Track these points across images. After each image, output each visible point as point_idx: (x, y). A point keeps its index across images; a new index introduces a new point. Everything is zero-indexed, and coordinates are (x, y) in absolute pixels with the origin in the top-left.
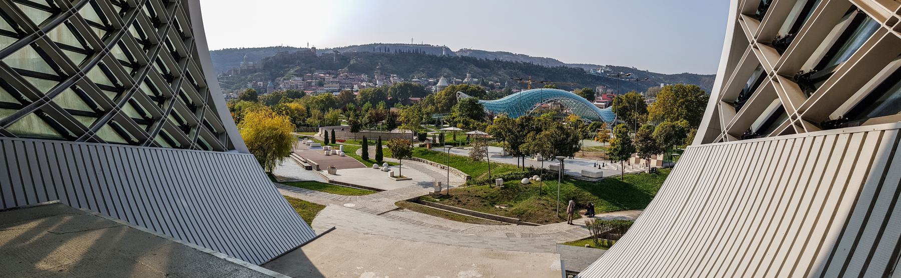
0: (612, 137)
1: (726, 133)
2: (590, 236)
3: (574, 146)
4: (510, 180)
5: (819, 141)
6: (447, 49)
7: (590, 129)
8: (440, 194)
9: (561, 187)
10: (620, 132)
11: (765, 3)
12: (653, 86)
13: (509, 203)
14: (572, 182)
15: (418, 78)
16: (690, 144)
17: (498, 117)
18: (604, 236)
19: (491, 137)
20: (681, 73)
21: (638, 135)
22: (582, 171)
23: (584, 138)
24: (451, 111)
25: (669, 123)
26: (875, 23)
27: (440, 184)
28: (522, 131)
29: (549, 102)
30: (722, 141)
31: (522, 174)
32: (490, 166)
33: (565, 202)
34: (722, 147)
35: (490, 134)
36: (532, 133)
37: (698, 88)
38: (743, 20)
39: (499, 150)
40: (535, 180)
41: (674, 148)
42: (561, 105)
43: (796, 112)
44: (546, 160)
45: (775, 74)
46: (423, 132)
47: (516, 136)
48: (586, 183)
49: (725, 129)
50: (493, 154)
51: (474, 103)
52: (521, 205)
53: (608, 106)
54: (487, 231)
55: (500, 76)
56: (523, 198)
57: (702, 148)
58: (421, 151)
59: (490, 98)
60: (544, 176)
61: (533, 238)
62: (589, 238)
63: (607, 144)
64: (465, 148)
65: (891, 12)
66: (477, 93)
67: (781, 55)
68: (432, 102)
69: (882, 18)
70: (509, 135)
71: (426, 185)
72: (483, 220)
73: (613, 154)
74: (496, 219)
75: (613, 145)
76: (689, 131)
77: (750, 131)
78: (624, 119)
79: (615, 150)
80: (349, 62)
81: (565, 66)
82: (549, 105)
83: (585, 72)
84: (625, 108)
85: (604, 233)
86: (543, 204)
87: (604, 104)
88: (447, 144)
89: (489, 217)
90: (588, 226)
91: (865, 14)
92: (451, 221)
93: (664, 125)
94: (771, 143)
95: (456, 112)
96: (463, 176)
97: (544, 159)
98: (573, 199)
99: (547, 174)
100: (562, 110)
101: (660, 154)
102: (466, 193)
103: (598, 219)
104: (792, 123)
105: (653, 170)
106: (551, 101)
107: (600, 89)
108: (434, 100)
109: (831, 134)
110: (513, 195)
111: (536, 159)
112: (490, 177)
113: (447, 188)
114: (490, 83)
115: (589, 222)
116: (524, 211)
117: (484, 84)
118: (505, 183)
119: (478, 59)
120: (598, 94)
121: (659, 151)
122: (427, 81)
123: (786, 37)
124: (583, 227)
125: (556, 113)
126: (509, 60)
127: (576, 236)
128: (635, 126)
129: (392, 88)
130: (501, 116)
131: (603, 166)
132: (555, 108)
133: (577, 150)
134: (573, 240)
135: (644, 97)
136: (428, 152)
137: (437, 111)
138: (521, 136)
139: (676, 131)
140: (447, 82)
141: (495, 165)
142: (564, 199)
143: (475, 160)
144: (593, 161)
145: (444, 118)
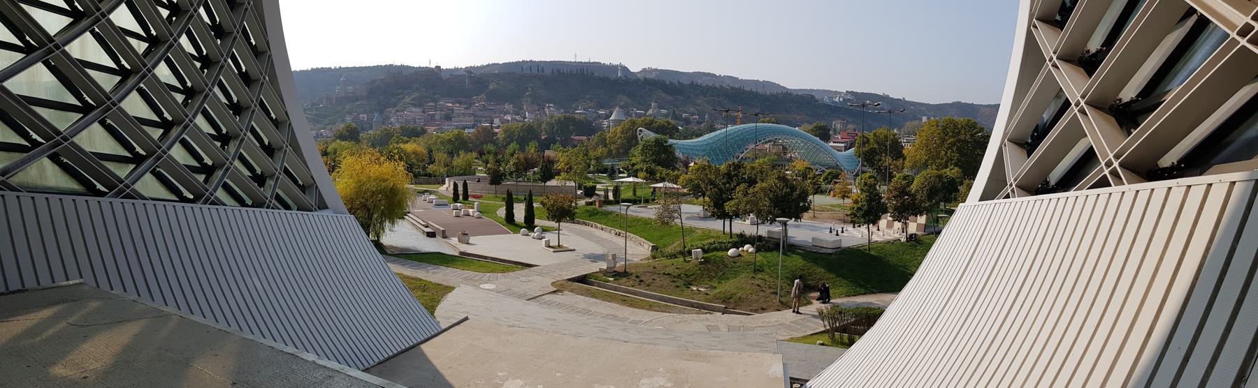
0: (855, 191)
1: (1014, 186)
2: (823, 329)
4: (712, 251)
5: (1143, 196)
6: (625, 69)
7: (824, 180)
8: (615, 271)
9: (783, 261)
10: (866, 184)
11: (1068, 5)
12: (911, 120)
13: (710, 283)
14: (798, 254)
15: (585, 110)
17: (695, 163)
18: (843, 329)
19: (685, 190)
21: (891, 188)
22: (813, 238)
25: (935, 171)
27: (614, 256)
28: (728, 182)
29: (766, 143)
30: (1008, 197)
32: (684, 232)
33: (788, 282)
34: (1008, 205)
35: (684, 187)
36: (743, 186)
37: (975, 123)
39: (697, 209)
41: (942, 207)
42: (783, 146)
43: (1111, 156)
44: (763, 223)
45: (1082, 103)
46: (591, 184)
47: (720, 190)
49: (1012, 181)
50: (689, 215)
51: (663, 144)
52: (728, 286)
54: (679, 322)
55: (699, 105)
62: (822, 332)
63: (847, 201)
64: (649, 207)
68: (603, 142)
69: (1231, 26)
70: (711, 189)
71: (595, 258)
72: (674, 307)
73: (856, 216)
74: (692, 305)
75: (856, 202)
76: (961, 184)
78: (872, 165)
81: (789, 92)
82: (767, 146)
83: (817, 101)
86: (759, 285)
87: (843, 145)
90: (821, 315)
93: (927, 174)
94: (1076, 199)
95: (636, 156)
96: (646, 246)
97: (759, 222)
98: (800, 278)
99: (763, 242)
100: (785, 154)
101: (921, 215)
102: (651, 269)
103: (836, 306)
104: (1106, 172)
105: (911, 238)
106: (769, 141)
107: (837, 124)
108: (606, 139)
109: (1161, 186)
111: (748, 222)
112: (685, 247)
113: (624, 263)
117: (676, 117)
119: (668, 83)
120: (835, 130)
123: (1098, 52)
124: (814, 316)
125: (776, 157)
126: (710, 84)
127: (804, 329)
128: (886, 176)
129: (547, 123)
130: (699, 161)
131: (843, 232)
133: (806, 209)
135: (900, 135)
137: (610, 154)
139: (944, 183)
141: (692, 230)
142: (787, 278)
143: (663, 223)
144: (829, 225)
145: (620, 165)
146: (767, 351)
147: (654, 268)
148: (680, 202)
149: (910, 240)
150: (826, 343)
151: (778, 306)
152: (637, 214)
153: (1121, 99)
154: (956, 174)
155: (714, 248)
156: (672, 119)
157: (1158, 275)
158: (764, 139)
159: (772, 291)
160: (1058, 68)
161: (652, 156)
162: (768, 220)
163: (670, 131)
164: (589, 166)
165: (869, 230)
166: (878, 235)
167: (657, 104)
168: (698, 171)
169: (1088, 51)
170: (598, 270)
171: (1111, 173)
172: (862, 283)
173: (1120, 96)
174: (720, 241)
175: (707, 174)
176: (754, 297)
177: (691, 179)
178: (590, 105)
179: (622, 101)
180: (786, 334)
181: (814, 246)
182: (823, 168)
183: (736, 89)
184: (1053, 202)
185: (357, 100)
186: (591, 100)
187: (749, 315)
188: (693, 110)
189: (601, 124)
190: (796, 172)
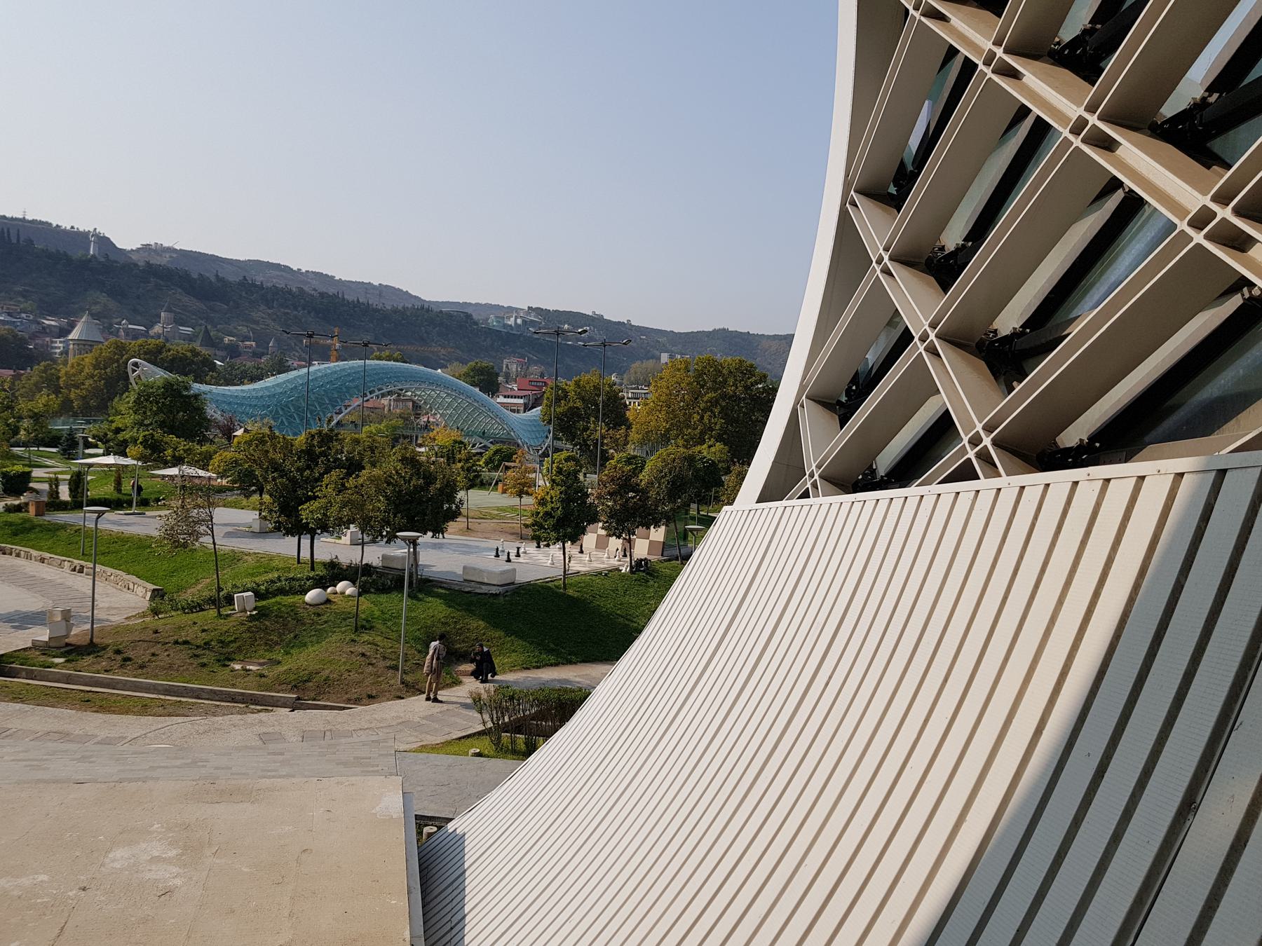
0: (541, 483)
1: (816, 477)
2: (481, 728)
3: (446, 506)
4: (275, 595)
5: (1032, 496)
6: (104, 242)
7: (487, 464)
8: (67, 645)
9: (410, 609)
10: (560, 471)
11: (910, 168)
12: (641, 359)
13: (269, 656)
14: (439, 596)
15: (9, 314)
16: (731, 502)
17: (246, 431)
18: (516, 727)
19: (224, 482)
21: (605, 478)
22: (465, 568)
23: (471, 487)
24: (111, 411)
25: (682, 450)
26: (1165, 220)
27: (67, 615)
28: (308, 467)
29: (383, 395)
30: (805, 495)
31: (308, 579)
32: (218, 560)
33: (419, 647)
34: (806, 509)
35: (222, 475)
36: (335, 474)
37: (751, 366)
38: (857, 206)
39: (249, 517)
40: (343, 593)
41: (693, 512)
42: (414, 402)
43: (979, 427)
44: (374, 541)
45: (932, 336)
46: (19, 468)
47: (293, 480)
48: (474, 599)
49: (814, 467)
50: (230, 529)
51: (179, 392)
52: (304, 659)
53: (533, 407)
54: (205, 732)
55: (257, 323)
56: (307, 640)
57: (759, 512)
58: (11, 524)
59: (225, 380)
60: (366, 582)
61: (333, 741)
62: (480, 733)
63: (528, 501)
64: (148, 513)
65: (1199, 196)
66: (189, 364)
67: (945, 290)
68: (53, 384)
69: (1180, 210)
70: (274, 479)
71: (23, 620)
72: (194, 704)
73: (541, 527)
74: (233, 698)
75: (542, 502)
76: (728, 471)
77: (873, 472)
78: (571, 437)
79: (548, 515)
81: (426, 306)
82: (385, 401)
83: (476, 323)
84: (573, 414)
85: (518, 720)
86: (363, 655)
87: (521, 401)
88: (93, 502)
89: (214, 695)
90: (477, 703)
91: (1142, 199)
92: (100, 715)
93: (669, 455)
94: (841, 506)
95: (124, 414)
96: (140, 591)
97: (366, 539)
98: (442, 637)
99: (374, 577)
100: (417, 416)
101: (657, 526)
102: (149, 635)
103: (504, 686)
104: (971, 454)
105: (640, 566)
106: (390, 393)
107: (512, 365)
108: (58, 378)
109: (1060, 479)
110: (280, 635)
111: (346, 540)
112: (220, 589)
113: (88, 626)
114: (226, 340)
115: (479, 695)
116: (311, 674)
117: (209, 341)
118: (260, 604)
119: (195, 276)
120: (507, 376)
121: (654, 519)
122: (38, 323)
123: (959, 249)
124: (465, 706)
125: (401, 422)
126: (281, 284)
127: (447, 730)
128: (597, 457)
130: (254, 428)
131: (518, 555)
132: (398, 411)
133: (453, 515)
134: (439, 740)
135: (621, 384)
136: (33, 527)
137: (66, 408)
138: (307, 481)
139: (698, 470)
140: (102, 332)
141: (235, 558)
142: (416, 639)
143: (177, 544)
144: (494, 544)
145: (85, 429)
146: (378, 771)
147: (156, 632)
148: (211, 505)
149: (638, 570)
150: (486, 752)
151: (399, 690)
152: (121, 529)
153: (996, 330)
154: (718, 455)
155: (278, 590)
156: (201, 345)
157: (1054, 631)
158: (379, 390)
159: (389, 663)
160: (891, 275)
161: (156, 414)
162: (382, 536)
163: (201, 369)
164: (16, 431)
165: (564, 554)
166: (581, 562)
167: (171, 315)
168: (250, 445)
169: (942, 248)
170: (29, 645)
171: (978, 455)
172: (552, 646)
173: (996, 325)
174: (291, 575)
175: (267, 452)
176: (354, 676)
177: (236, 461)
179: (96, 303)
180: (413, 739)
181: (466, 580)
182: (485, 443)
183: (330, 296)
184: (883, 505)
186: (24, 296)
187: (344, 708)
188: (245, 330)
189: (48, 346)
190: (436, 448)
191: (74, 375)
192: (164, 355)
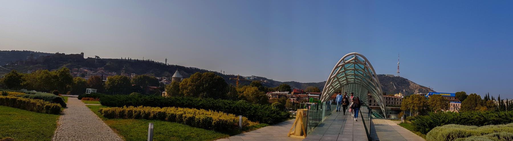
20: (290, 81)
80: (105, 64)
129: (134, 79)
178: (152, 75)
185: (37, 64)
191: (184, 85)
192: (215, 77)
